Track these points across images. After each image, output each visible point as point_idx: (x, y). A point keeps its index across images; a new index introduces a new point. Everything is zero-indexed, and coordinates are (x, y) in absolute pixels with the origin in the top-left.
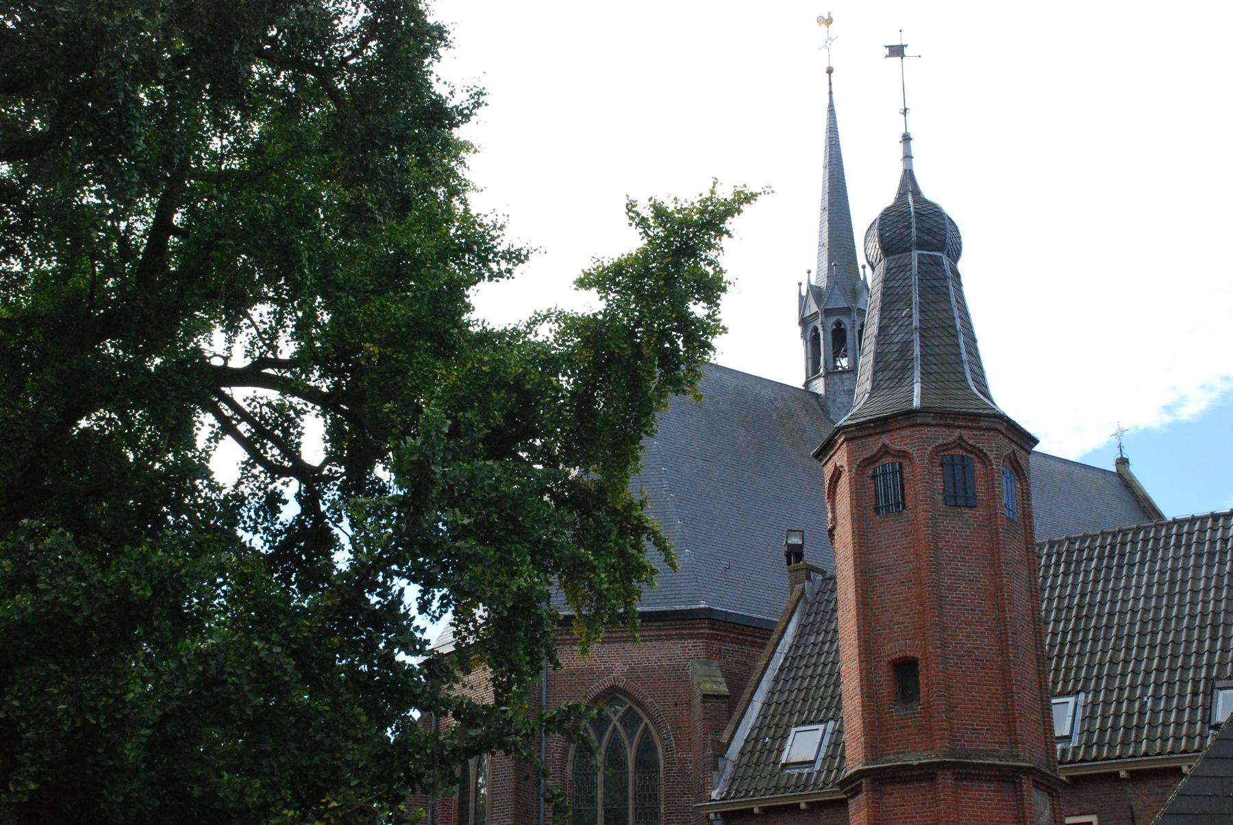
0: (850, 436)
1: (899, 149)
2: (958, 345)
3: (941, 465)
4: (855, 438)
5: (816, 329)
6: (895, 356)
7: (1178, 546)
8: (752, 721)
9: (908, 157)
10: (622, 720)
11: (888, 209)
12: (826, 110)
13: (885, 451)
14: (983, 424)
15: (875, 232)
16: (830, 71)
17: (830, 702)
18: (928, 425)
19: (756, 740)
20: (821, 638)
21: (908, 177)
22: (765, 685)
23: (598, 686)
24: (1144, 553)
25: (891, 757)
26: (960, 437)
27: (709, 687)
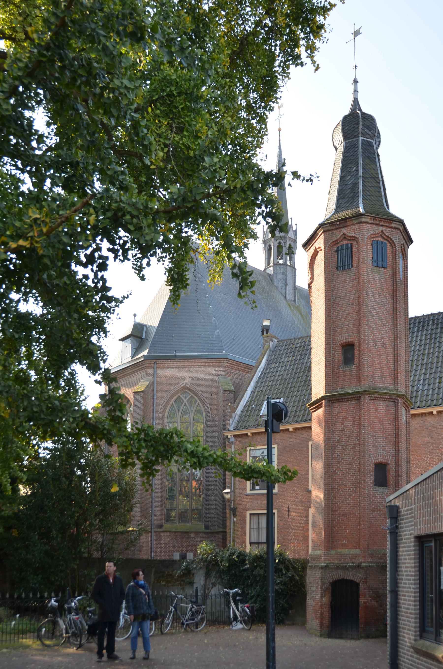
0: (325, 229)
1: (353, 86)
2: (380, 187)
3: (372, 245)
4: (329, 230)
5: (270, 246)
6: (348, 191)
7: (433, 324)
8: (247, 398)
9: (356, 91)
10: (188, 401)
11: (346, 116)
12: (277, 147)
13: (345, 237)
14: (393, 225)
15: (340, 127)
16: (280, 130)
17: (282, 391)
18: (367, 223)
19: (249, 407)
20: (277, 365)
21: (356, 102)
22: (252, 384)
23: (178, 386)
24: (419, 328)
25: (338, 390)
26: (382, 231)
27: (227, 387)
